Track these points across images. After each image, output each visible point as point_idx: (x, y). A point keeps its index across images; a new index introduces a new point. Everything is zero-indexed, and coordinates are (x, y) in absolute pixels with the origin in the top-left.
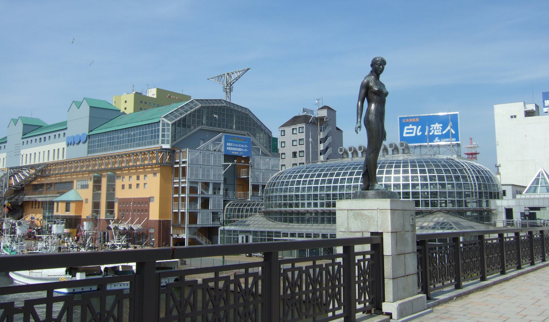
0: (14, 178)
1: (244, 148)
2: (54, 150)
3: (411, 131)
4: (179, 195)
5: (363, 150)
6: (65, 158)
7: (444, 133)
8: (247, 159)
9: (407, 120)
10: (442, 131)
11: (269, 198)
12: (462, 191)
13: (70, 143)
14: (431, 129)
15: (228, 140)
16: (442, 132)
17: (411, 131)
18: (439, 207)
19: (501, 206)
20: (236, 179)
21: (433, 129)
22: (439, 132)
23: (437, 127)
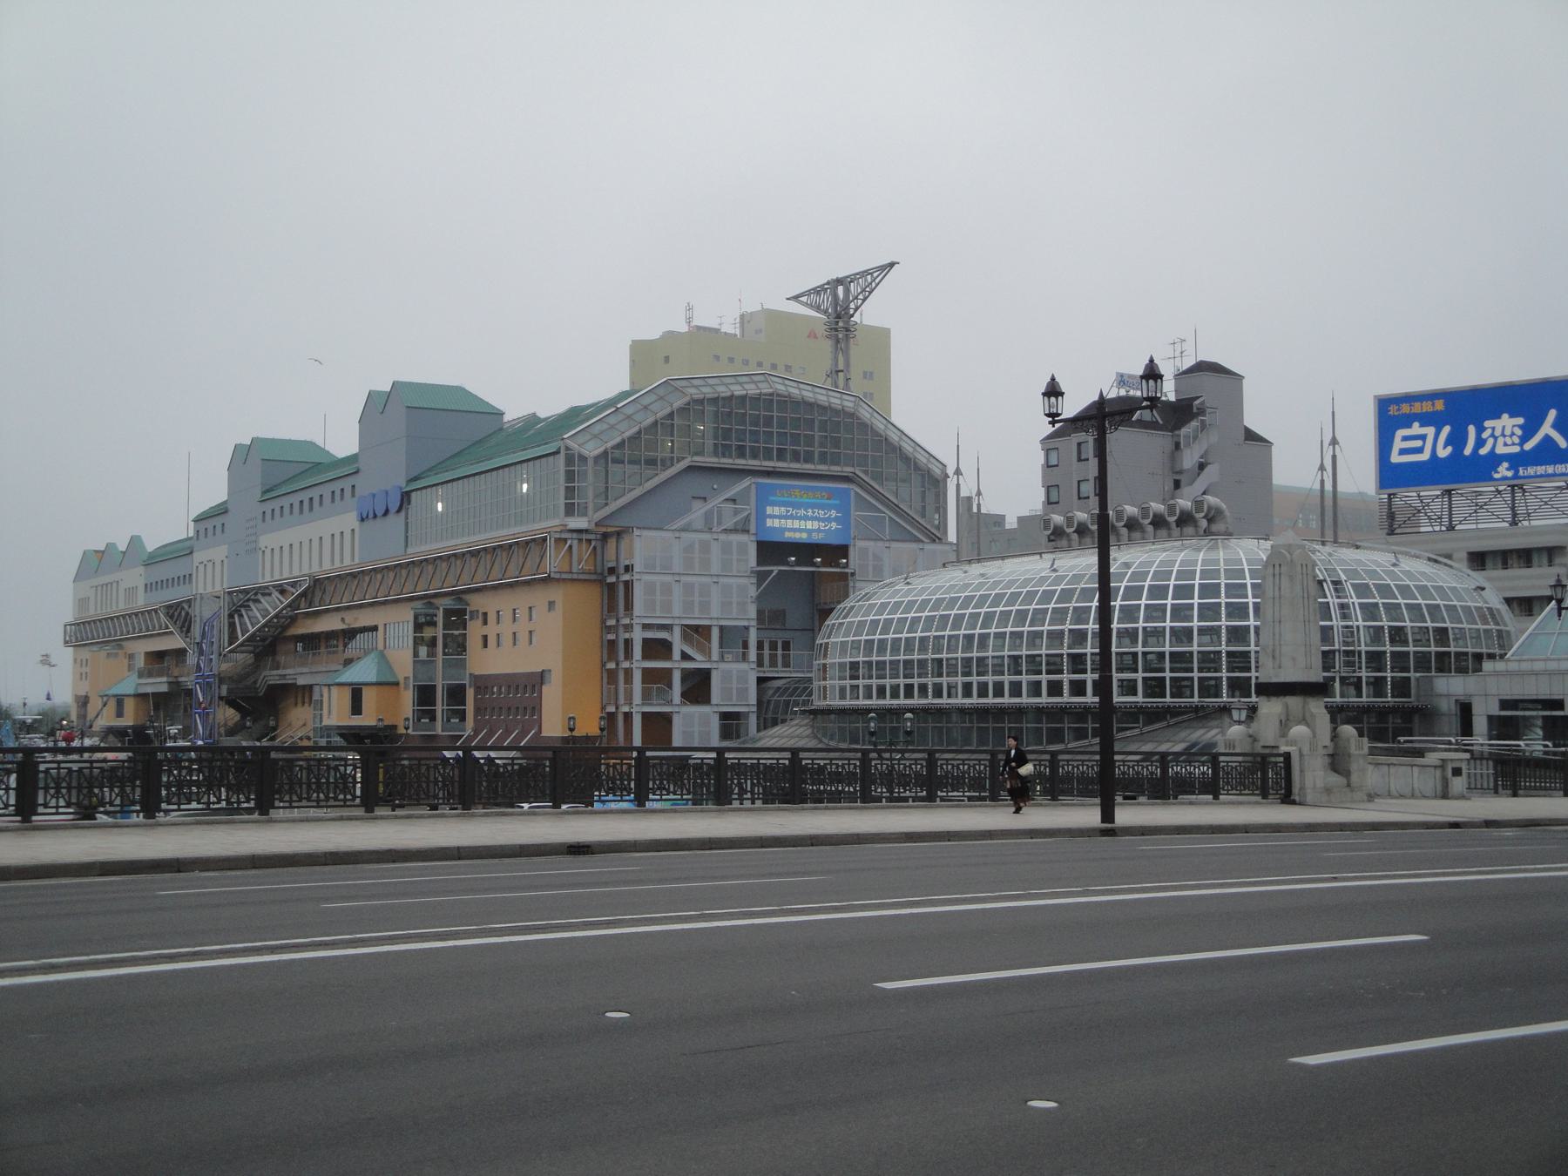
0: (250, 613)
1: (829, 520)
2: (333, 535)
3: (1418, 443)
4: (617, 664)
5: (1075, 525)
6: (357, 561)
7: (1528, 446)
8: (842, 551)
9: (1406, 409)
10: (1524, 439)
11: (825, 671)
12: (1383, 649)
13: (364, 516)
14: (1485, 435)
15: (772, 498)
16: (1521, 444)
17: (1418, 443)
18: (1196, 699)
19: (1448, 696)
20: (815, 611)
21: (1492, 435)
22: (1513, 444)
23: (1504, 427)
